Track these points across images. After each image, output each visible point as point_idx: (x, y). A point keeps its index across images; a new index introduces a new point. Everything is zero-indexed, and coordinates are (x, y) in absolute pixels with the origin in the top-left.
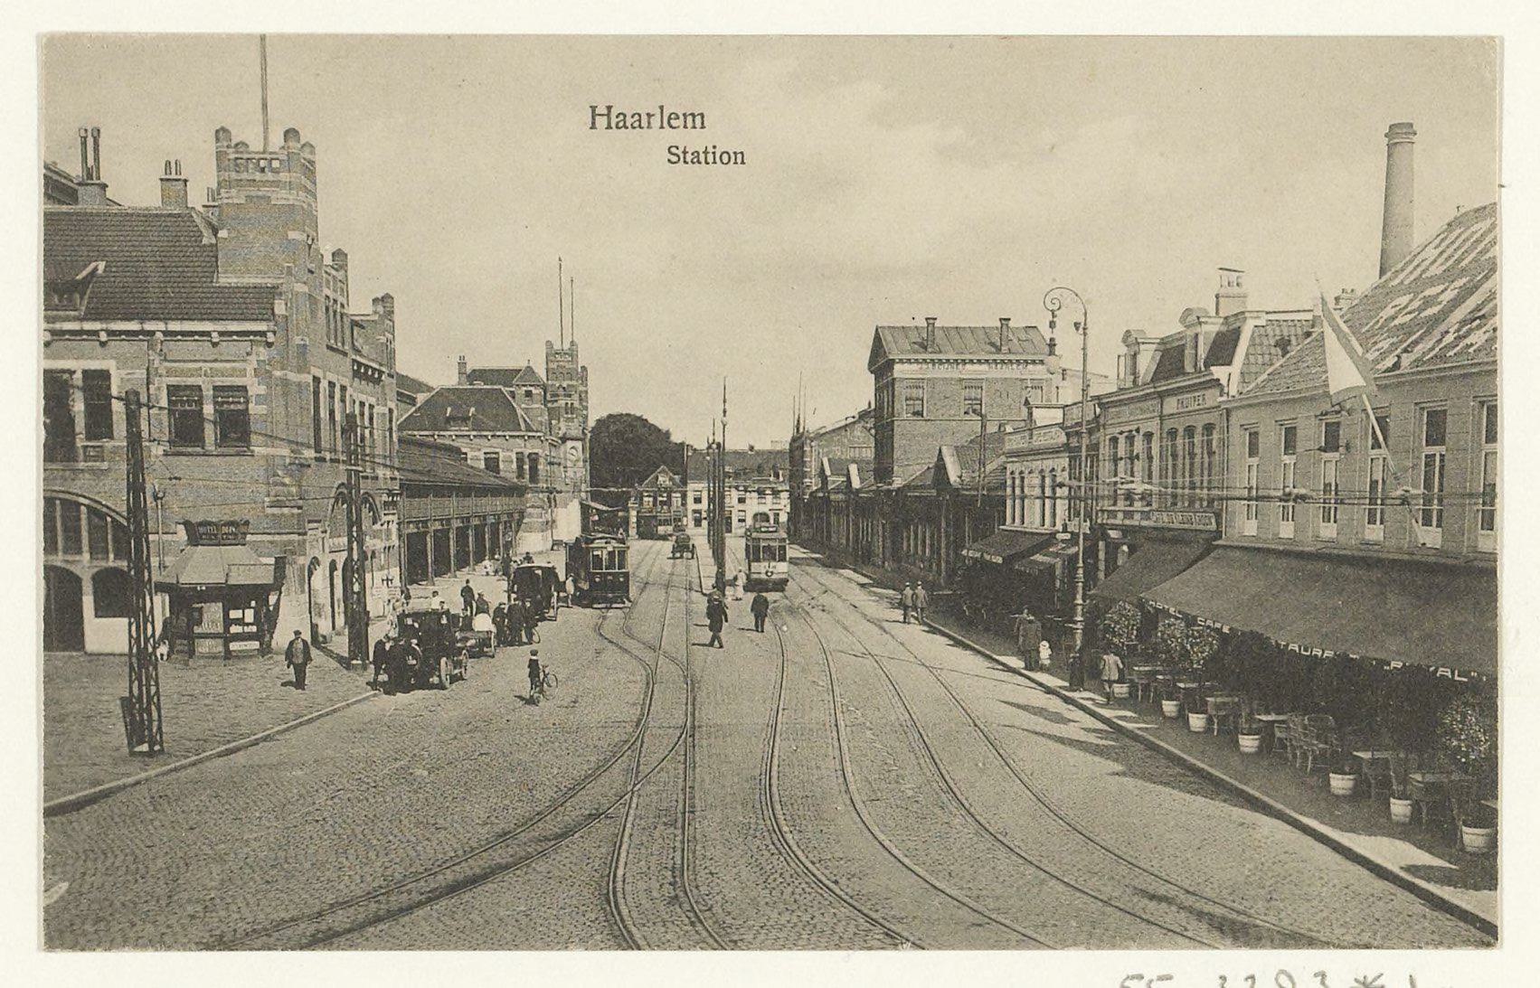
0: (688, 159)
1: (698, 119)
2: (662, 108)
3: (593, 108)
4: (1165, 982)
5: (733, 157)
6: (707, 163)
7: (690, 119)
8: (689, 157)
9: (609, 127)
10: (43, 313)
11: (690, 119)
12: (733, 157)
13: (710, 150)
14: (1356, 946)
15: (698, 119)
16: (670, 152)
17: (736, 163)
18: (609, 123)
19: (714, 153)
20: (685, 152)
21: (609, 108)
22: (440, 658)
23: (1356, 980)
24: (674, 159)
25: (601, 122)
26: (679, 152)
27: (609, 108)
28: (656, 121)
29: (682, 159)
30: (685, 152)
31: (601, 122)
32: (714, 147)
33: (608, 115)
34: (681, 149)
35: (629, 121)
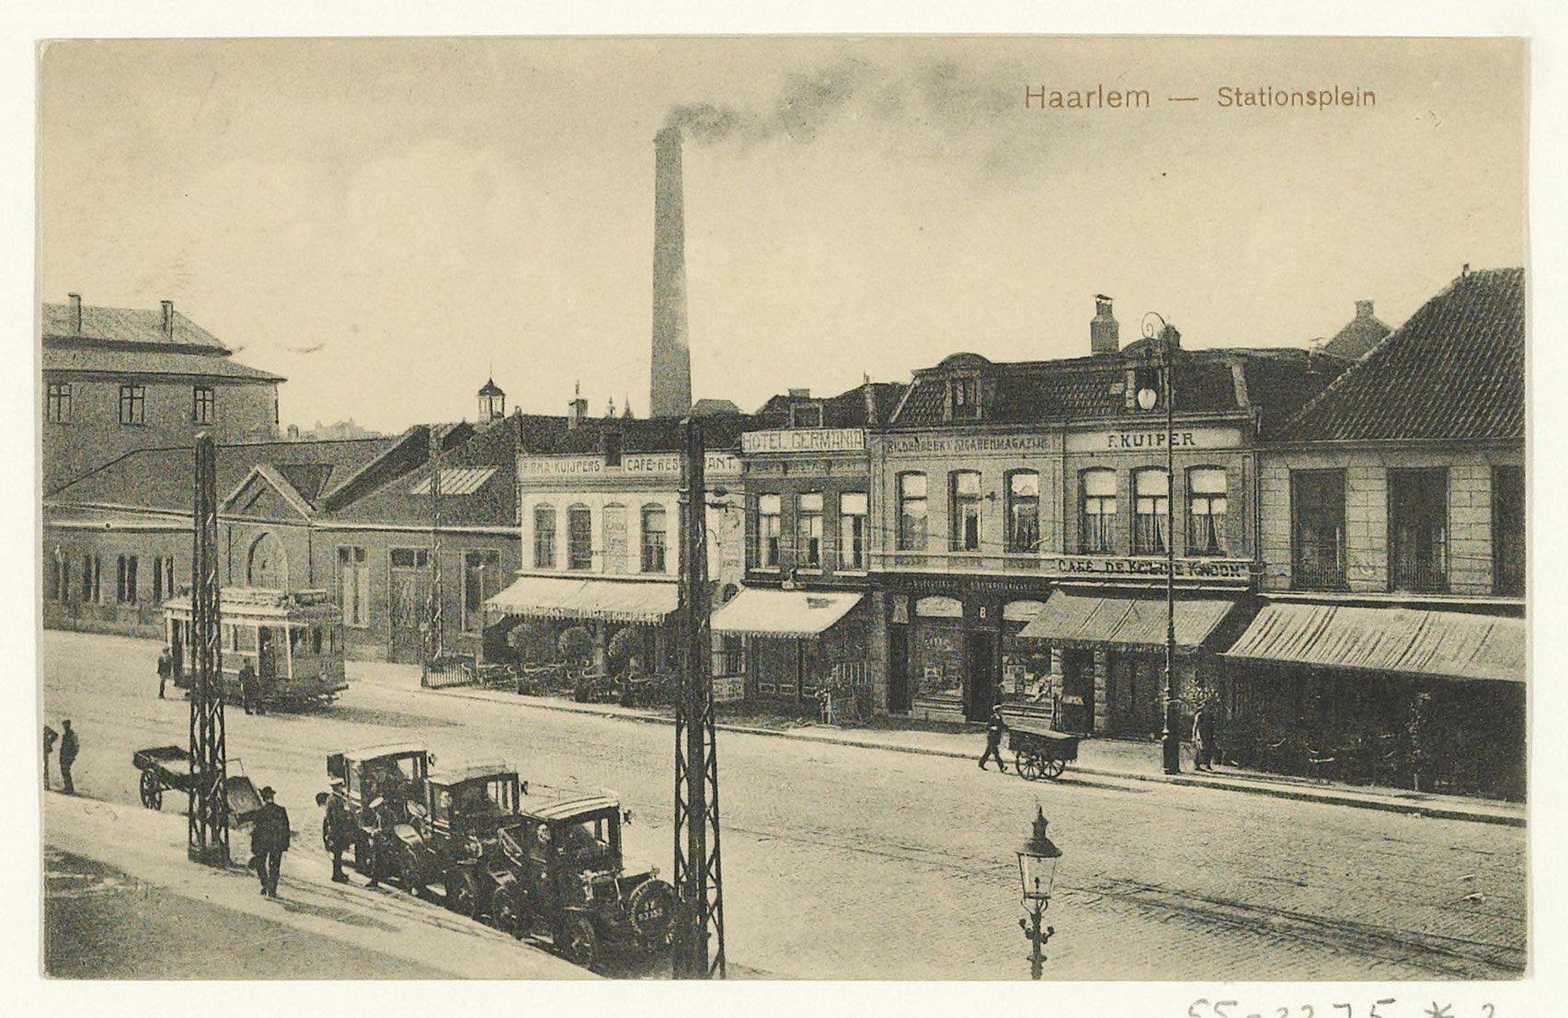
1: (1143, 98)
7: (1133, 98)
11: (1133, 98)
13: (1266, 90)
15: (1143, 98)
20: (1238, 94)
28: (1095, 100)
29: (1235, 102)
30: (1238, 94)
34: (1235, 91)
35: (1066, 98)
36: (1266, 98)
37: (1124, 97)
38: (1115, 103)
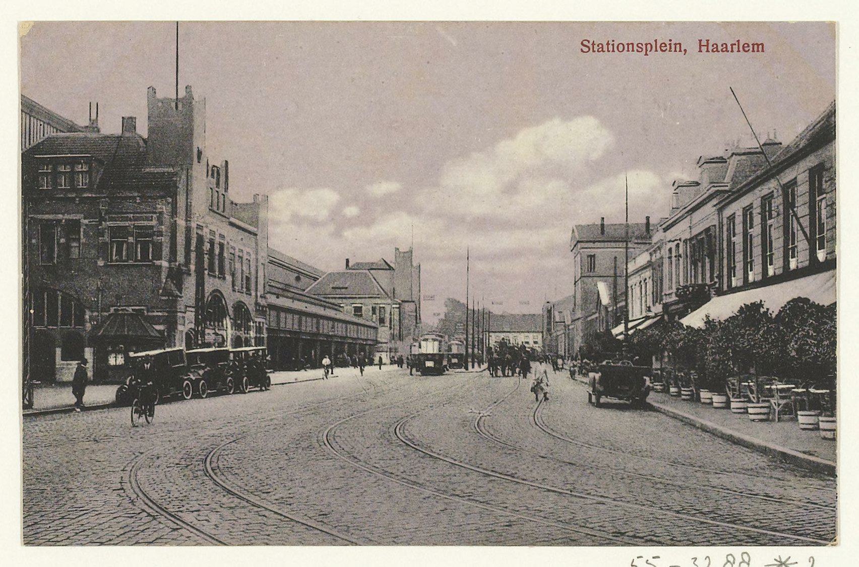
0: (596, 49)
1: (761, 46)
2: (738, 41)
3: (700, 41)
4: (640, 559)
5: (626, 47)
6: (608, 51)
8: (596, 48)
9: (708, 51)
10: (837, 317)
12: (626, 47)
13: (611, 43)
14: (806, 546)
16: (582, 44)
17: (628, 51)
18: (708, 49)
19: (613, 45)
20: (593, 44)
21: (708, 41)
22: (311, 350)
23: (775, 560)
24: (586, 49)
25: (704, 49)
26: (590, 45)
27: (708, 41)
30: (593, 44)
31: (704, 49)
32: (613, 41)
33: (707, 46)
34: (591, 43)
36: (611, 48)
37: (751, 46)
38: (747, 49)
